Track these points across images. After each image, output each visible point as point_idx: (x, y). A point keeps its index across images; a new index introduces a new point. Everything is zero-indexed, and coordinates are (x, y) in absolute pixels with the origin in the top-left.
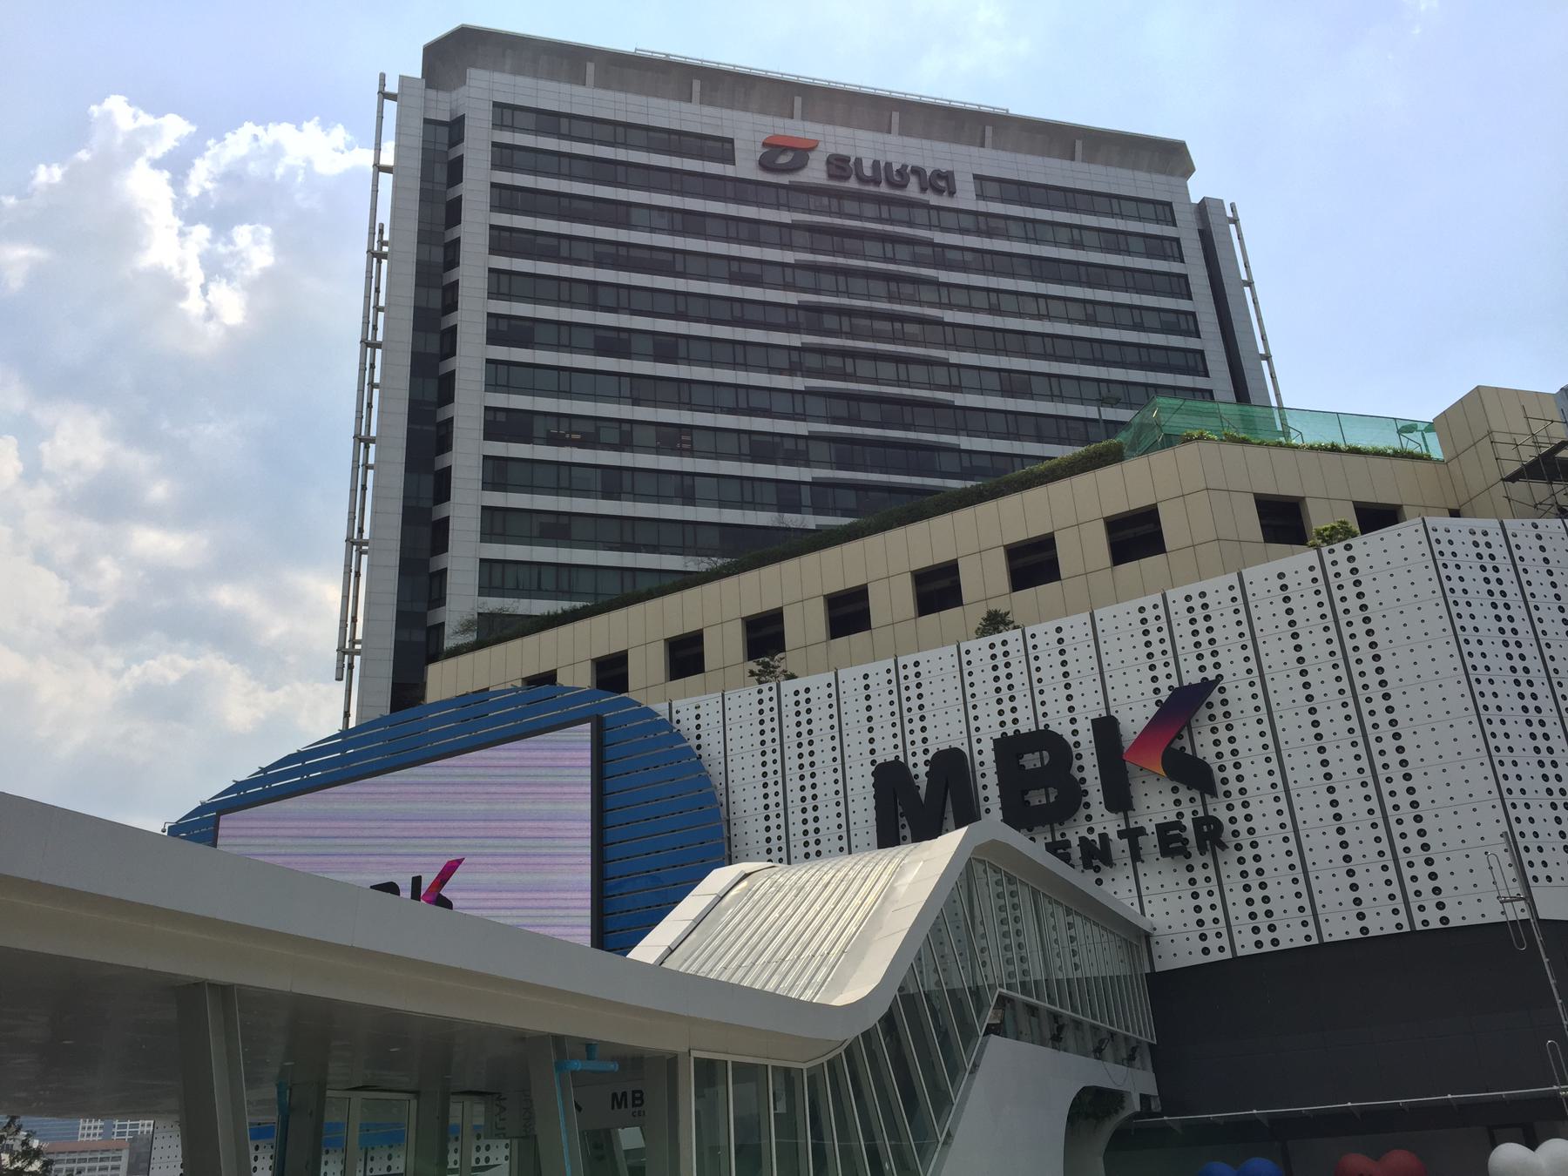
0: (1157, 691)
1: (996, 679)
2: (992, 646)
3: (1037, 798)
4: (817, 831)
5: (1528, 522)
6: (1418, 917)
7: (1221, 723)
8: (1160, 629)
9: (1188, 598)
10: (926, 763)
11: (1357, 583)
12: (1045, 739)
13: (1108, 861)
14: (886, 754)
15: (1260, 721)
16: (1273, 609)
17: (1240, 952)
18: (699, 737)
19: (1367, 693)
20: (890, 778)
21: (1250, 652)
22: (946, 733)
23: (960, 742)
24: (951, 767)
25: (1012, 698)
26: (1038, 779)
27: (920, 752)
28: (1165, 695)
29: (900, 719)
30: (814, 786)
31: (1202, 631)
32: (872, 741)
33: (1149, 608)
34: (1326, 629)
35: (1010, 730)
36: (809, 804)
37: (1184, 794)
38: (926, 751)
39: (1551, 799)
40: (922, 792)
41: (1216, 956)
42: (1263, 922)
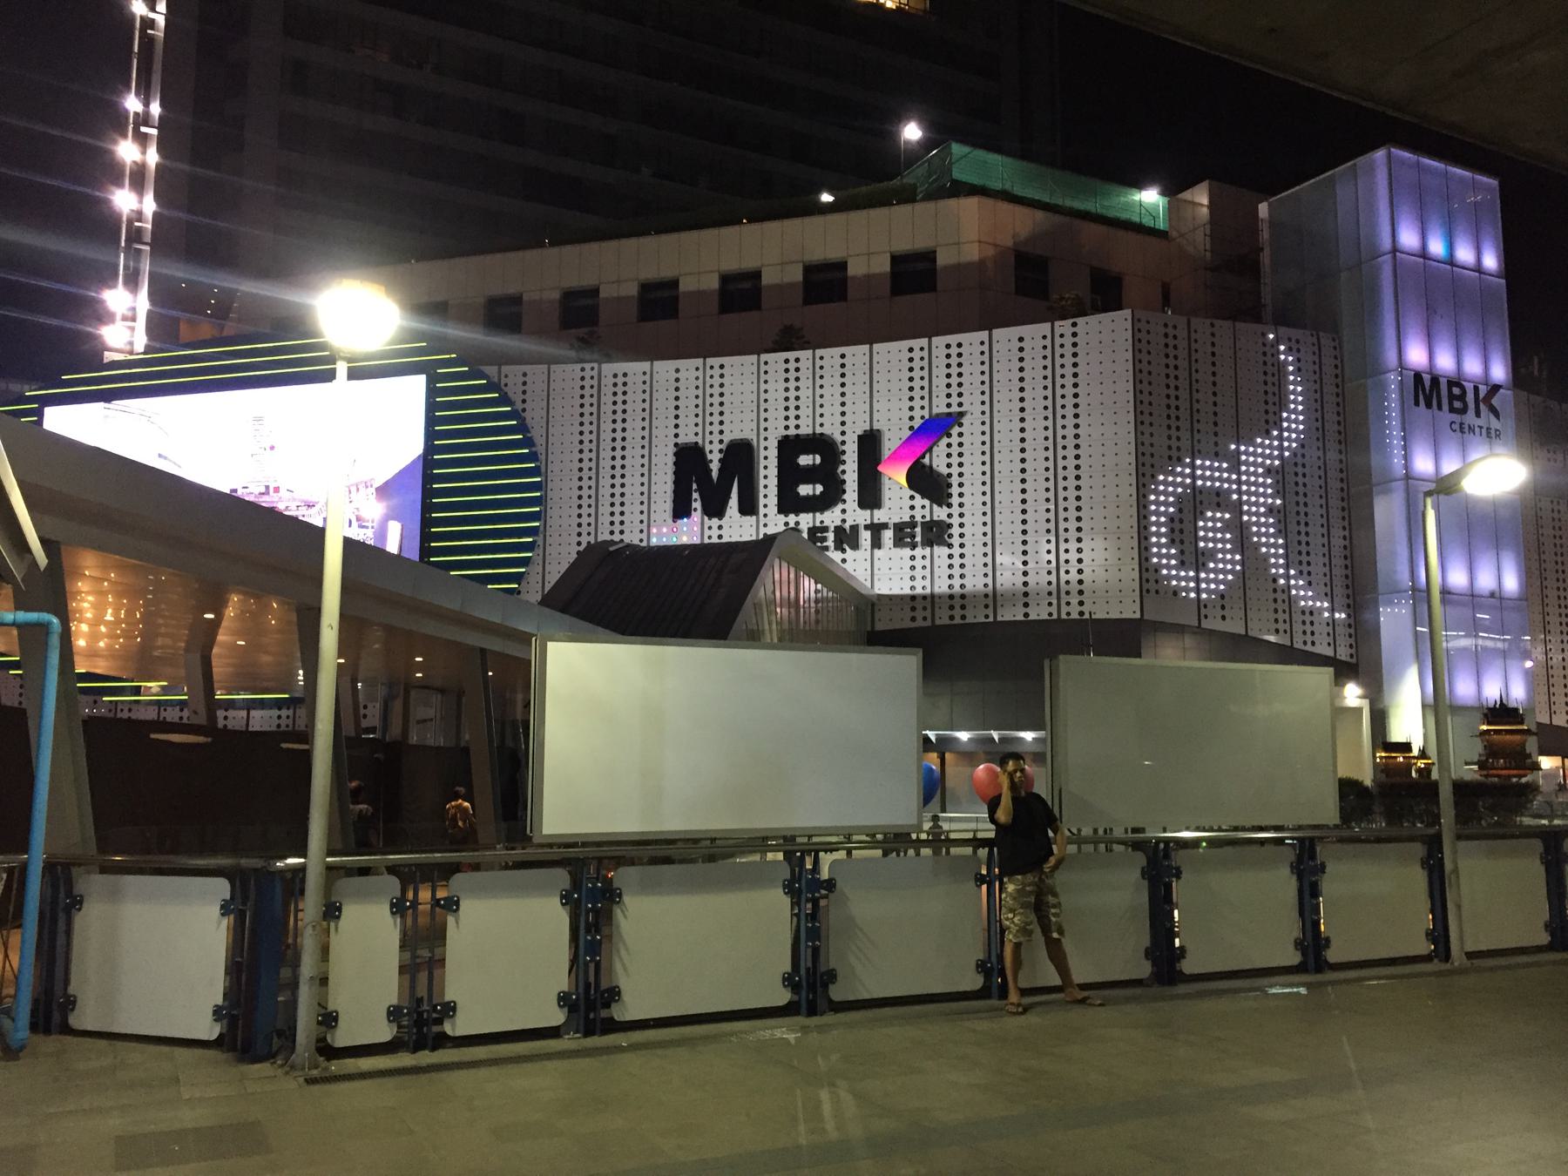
0: (911, 418)
1: (624, 402)
2: (787, 361)
3: (805, 490)
4: (623, 495)
5: (1208, 321)
6: (1064, 609)
7: (955, 450)
8: (1065, 478)
9: (948, 346)
10: (721, 451)
11: (1075, 355)
12: (826, 447)
13: (855, 546)
14: (687, 437)
15: (984, 494)
16: (1012, 456)
17: (938, 622)
18: (524, 401)
19: (1065, 473)
20: (689, 460)
21: (987, 458)
22: (739, 428)
23: (752, 436)
24: (740, 456)
25: (797, 408)
26: (809, 475)
27: (716, 442)
28: (917, 423)
29: (702, 411)
30: (623, 485)
31: (955, 454)
32: (677, 426)
33: (917, 350)
34: (1046, 418)
35: (792, 432)
36: (619, 416)
37: (919, 501)
38: (721, 442)
39: (1166, 391)
40: (715, 474)
41: (919, 623)
42: (957, 571)
